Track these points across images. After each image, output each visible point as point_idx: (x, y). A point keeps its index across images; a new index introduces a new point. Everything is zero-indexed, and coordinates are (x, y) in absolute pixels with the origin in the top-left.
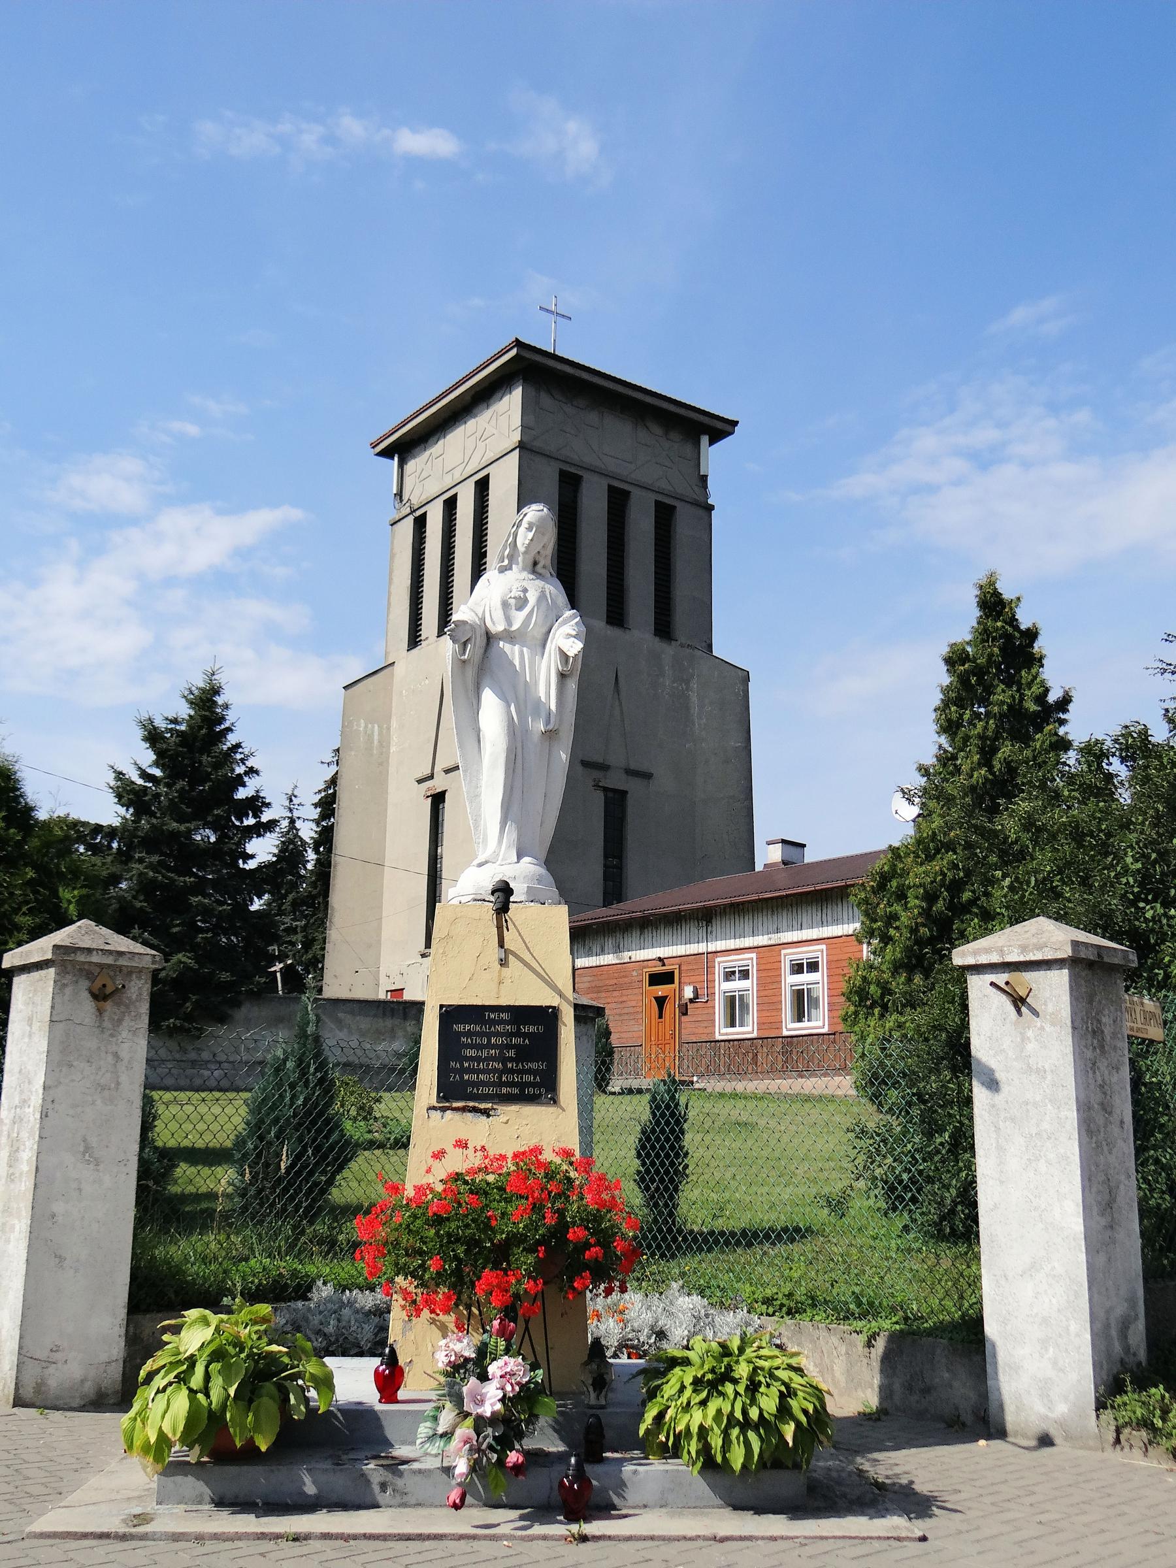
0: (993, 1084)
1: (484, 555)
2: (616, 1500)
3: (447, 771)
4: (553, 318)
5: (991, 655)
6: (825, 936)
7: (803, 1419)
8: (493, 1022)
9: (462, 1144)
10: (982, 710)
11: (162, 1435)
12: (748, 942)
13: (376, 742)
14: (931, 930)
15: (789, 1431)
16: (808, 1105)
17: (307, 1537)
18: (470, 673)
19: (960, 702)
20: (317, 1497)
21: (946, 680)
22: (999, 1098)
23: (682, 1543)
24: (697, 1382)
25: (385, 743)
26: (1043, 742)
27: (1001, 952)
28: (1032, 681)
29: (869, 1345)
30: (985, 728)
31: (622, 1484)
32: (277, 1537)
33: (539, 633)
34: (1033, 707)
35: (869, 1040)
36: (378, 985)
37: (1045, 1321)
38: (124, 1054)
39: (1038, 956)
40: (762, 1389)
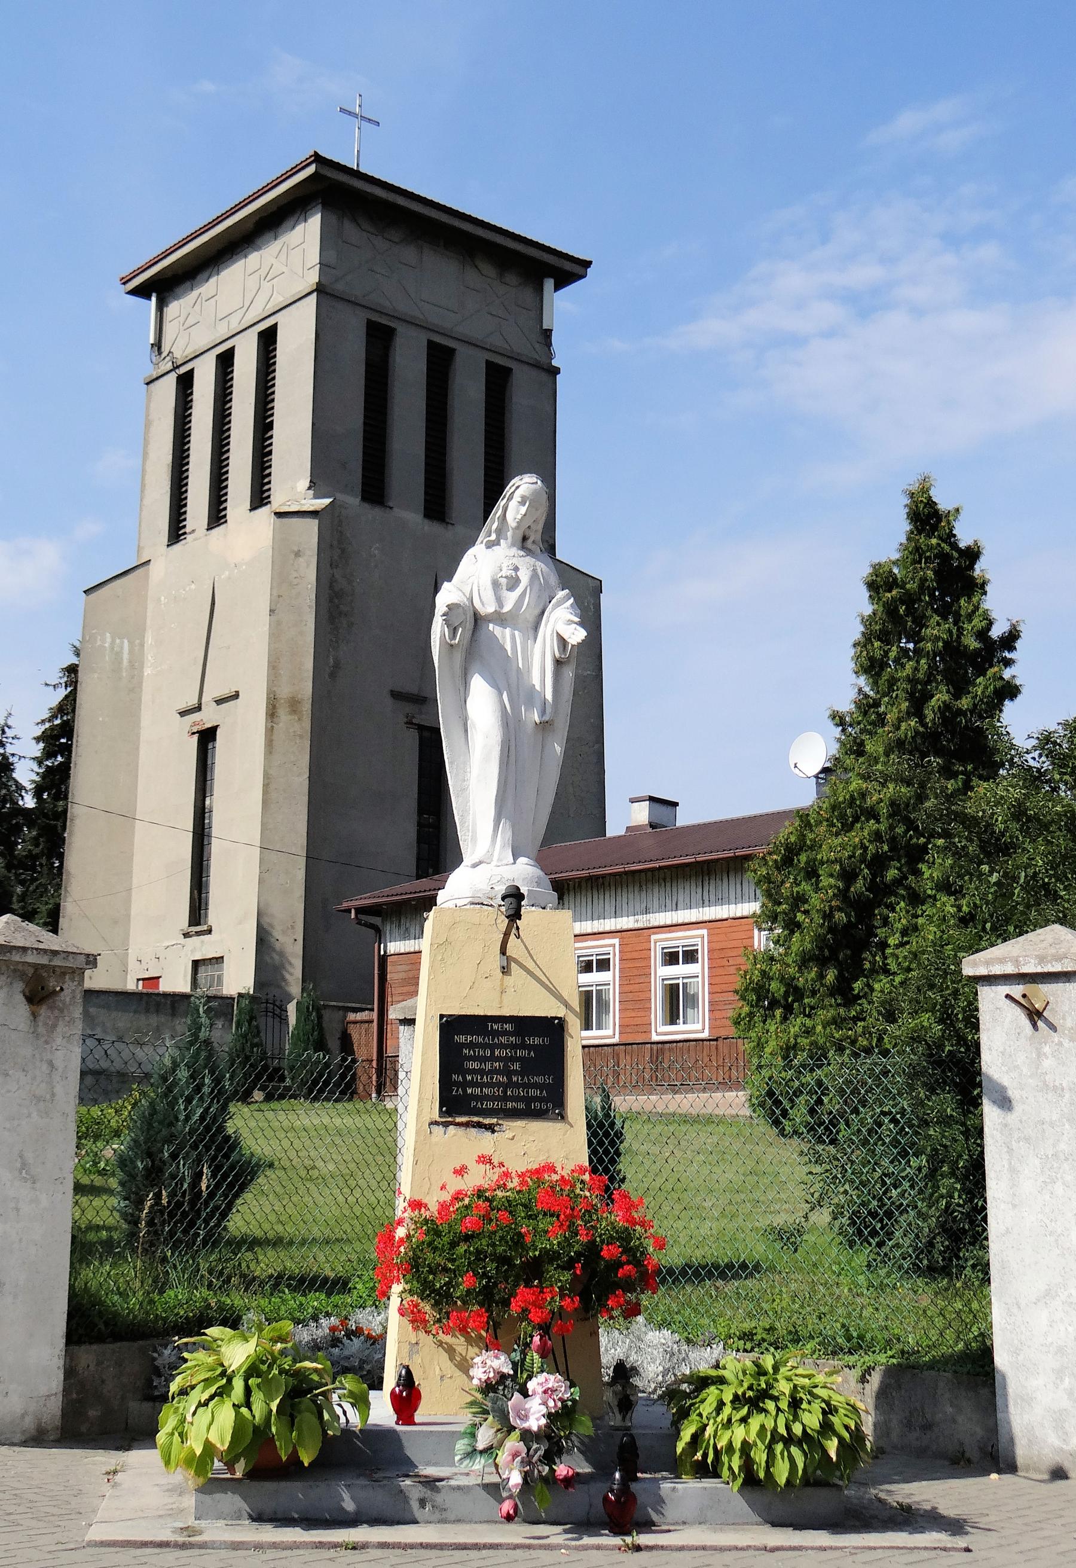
0: (1005, 1103)
1: (270, 426)
2: (655, 1517)
3: (219, 702)
4: (356, 122)
5: (924, 580)
6: (706, 918)
7: (846, 1435)
8: (496, 1034)
9: (484, 1160)
10: (911, 646)
11: (208, 1446)
12: (609, 924)
13: (125, 662)
14: (848, 915)
15: (832, 1447)
16: (697, 1126)
17: (364, 1546)
18: (458, 657)
19: (885, 637)
20: (357, 1513)
21: (868, 609)
22: (1012, 1118)
23: (734, 1552)
24: (736, 1398)
25: (137, 663)
26: (986, 688)
27: (1016, 962)
28: (974, 612)
29: (863, 1380)
30: (916, 669)
31: (661, 1501)
32: (335, 1546)
33: (531, 616)
34: (973, 644)
35: (768, 1050)
36: (125, 971)
37: (1061, 1351)
38: (59, 1063)
39: (1057, 968)
40: (804, 1406)
